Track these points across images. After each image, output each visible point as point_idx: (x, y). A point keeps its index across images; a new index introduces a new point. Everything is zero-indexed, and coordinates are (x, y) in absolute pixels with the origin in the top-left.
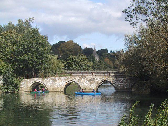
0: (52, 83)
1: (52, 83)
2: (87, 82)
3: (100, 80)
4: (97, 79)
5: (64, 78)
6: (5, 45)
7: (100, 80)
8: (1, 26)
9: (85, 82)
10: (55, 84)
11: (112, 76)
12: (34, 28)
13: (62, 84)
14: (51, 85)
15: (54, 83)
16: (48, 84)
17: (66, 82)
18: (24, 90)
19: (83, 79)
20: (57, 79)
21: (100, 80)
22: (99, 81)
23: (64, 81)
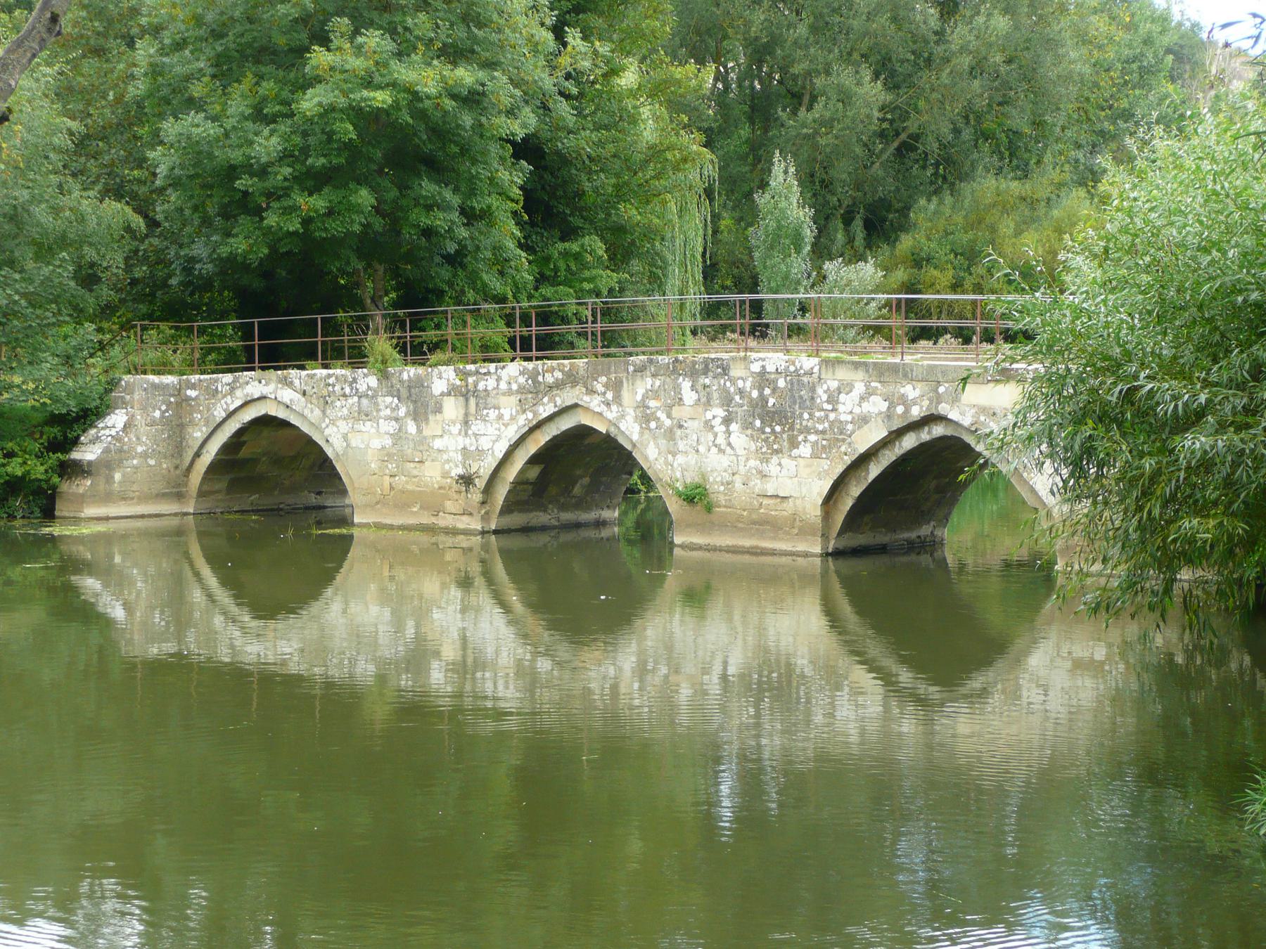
0: (391, 427)
1: (391, 427)
2: (734, 427)
3: (867, 407)
4: (833, 399)
5: (504, 374)
6: (99, 254)
7: (867, 407)
8: (956, 5)
9: (708, 426)
10: (422, 442)
11: (311, 85)
12: (357, 358)
13: (485, 443)
14: (386, 456)
15: (411, 427)
16: (355, 441)
17: (525, 420)
18: (108, 498)
19: (689, 396)
20: (439, 387)
21: (877, 405)
22: (864, 420)
23: (507, 413)
